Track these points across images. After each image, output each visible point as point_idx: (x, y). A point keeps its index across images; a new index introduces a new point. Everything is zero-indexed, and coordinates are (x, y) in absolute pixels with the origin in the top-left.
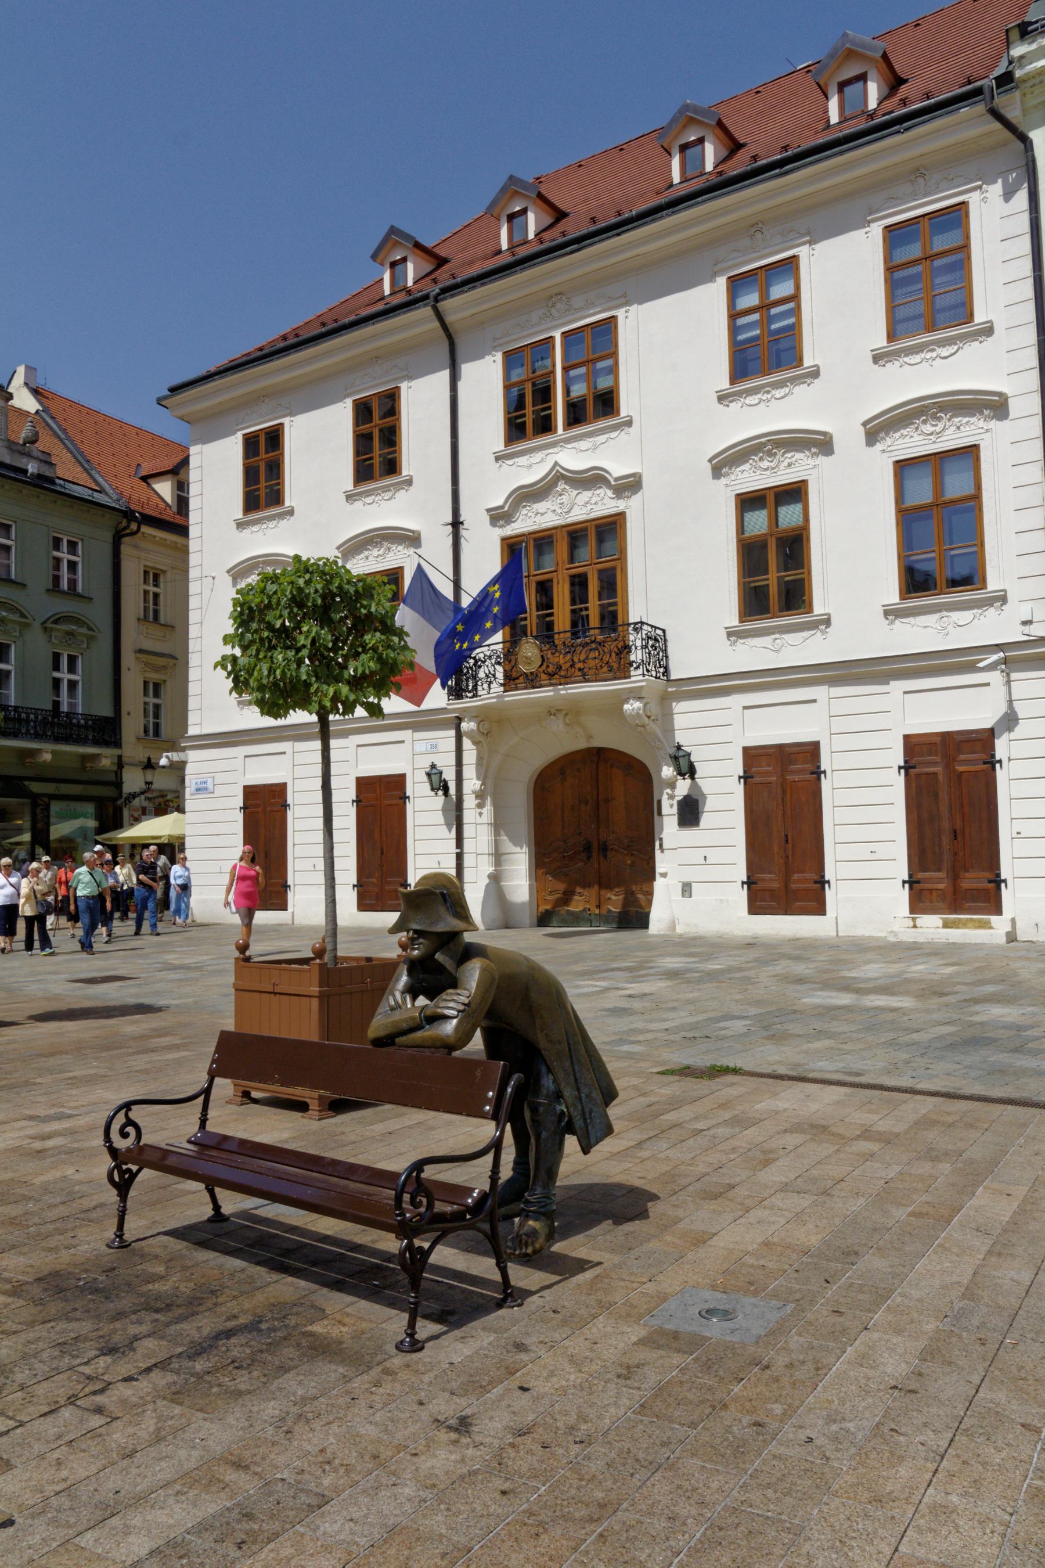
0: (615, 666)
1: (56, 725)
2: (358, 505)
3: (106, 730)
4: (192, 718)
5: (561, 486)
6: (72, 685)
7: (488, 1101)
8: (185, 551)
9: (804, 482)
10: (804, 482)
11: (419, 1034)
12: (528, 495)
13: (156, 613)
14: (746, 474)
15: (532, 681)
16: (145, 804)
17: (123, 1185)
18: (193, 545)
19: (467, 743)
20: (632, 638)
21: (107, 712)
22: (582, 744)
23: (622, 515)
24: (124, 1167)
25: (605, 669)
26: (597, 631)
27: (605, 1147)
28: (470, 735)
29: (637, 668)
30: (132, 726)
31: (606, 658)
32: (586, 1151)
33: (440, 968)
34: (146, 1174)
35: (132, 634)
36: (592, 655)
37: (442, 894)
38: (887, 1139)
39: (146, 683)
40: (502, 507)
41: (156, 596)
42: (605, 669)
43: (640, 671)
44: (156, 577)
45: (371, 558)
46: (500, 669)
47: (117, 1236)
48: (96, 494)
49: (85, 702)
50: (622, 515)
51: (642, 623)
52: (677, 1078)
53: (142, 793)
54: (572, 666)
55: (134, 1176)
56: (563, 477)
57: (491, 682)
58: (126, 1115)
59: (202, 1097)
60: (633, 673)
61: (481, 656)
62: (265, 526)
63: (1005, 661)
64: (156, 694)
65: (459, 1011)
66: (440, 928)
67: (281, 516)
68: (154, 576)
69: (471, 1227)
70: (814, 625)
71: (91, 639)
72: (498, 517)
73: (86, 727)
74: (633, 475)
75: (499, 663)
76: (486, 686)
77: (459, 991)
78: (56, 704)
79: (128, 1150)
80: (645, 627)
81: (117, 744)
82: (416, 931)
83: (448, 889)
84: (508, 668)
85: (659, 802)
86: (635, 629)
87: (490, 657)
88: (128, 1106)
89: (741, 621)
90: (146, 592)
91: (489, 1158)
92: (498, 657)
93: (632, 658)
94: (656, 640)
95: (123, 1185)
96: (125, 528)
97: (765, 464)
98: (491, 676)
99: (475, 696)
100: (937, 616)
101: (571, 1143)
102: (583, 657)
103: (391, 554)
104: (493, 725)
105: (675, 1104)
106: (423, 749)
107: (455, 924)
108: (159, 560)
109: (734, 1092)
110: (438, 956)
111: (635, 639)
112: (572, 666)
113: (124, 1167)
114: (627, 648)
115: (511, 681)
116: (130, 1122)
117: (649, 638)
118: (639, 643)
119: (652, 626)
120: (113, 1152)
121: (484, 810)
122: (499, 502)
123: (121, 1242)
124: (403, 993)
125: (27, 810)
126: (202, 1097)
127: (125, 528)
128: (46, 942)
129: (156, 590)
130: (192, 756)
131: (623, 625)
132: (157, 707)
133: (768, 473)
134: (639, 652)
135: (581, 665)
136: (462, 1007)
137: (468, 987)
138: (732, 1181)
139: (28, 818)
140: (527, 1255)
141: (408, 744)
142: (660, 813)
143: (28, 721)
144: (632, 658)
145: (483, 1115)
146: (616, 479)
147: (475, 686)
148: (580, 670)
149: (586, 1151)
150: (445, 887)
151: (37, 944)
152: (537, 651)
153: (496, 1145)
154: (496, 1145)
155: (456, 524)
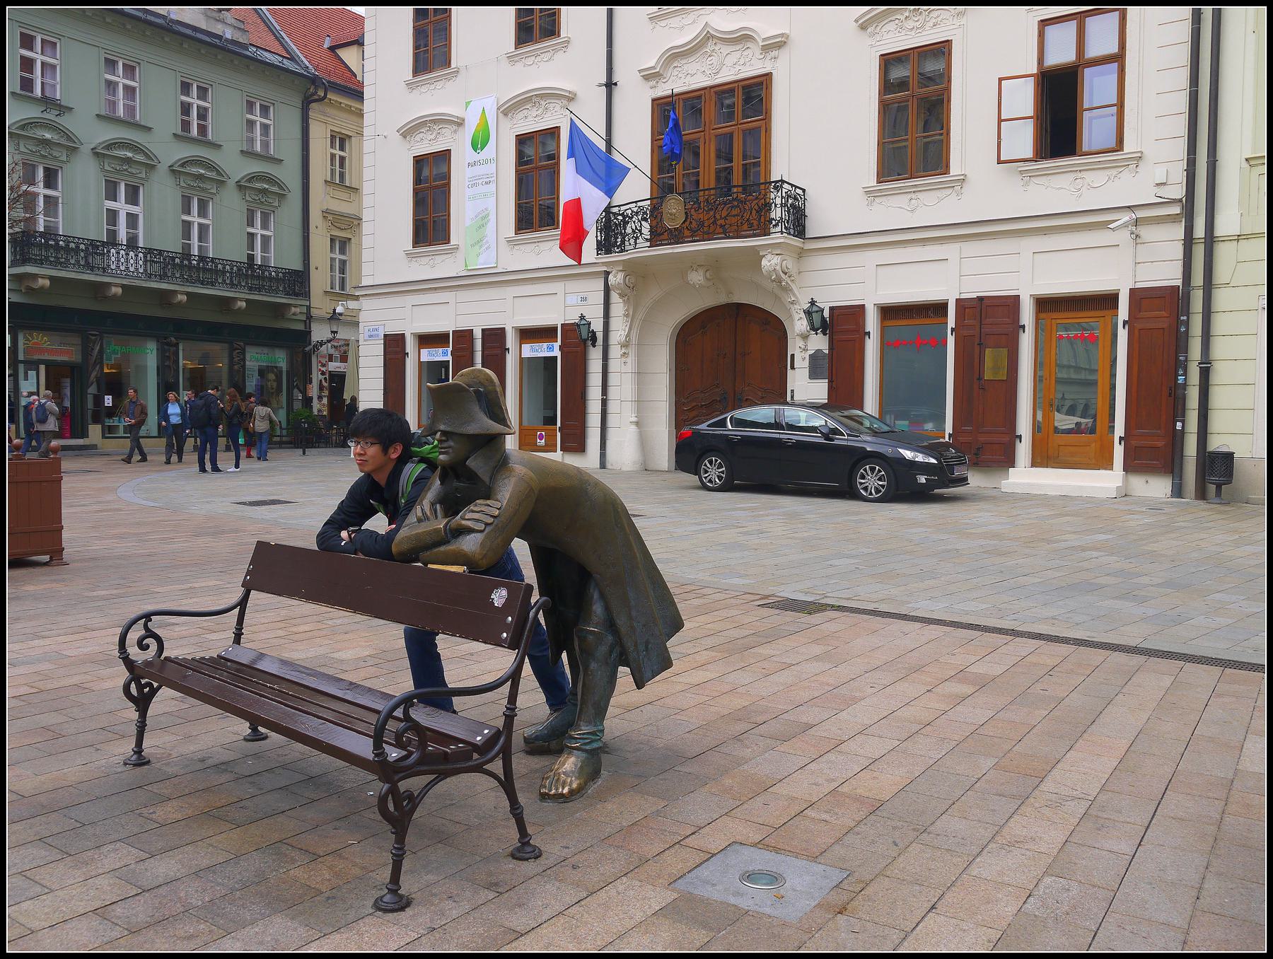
0: (755, 223)
1: (250, 273)
2: (519, 66)
3: (298, 281)
4: (366, 270)
5: (710, 47)
6: (266, 240)
7: (506, 628)
8: (360, 114)
9: (948, 42)
10: (948, 43)
11: (442, 548)
12: (675, 56)
13: (342, 175)
14: (891, 35)
15: (676, 237)
16: (332, 351)
17: (142, 702)
18: (368, 106)
19: (615, 297)
20: (772, 196)
21: (296, 265)
22: (722, 299)
23: (768, 76)
24: (143, 682)
25: (745, 227)
26: (740, 189)
27: (656, 686)
28: (618, 287)
29: (776, 225)
30: (320, 280)
31: (746, 215)
32: (640, 685)
33: (472, 477)
34: (165, 692)
35: (320, 198)
36: (735, 212)
37: (477, 392)
38: (983, 683)
39: (332, 240)
40: (653, 68)
41: (342, 159)
42: (745, 227)
43: (779, 229)
44: (342, 141)
45: (530, 118)
46: (646, 225)
47: (135, 753)
48: (285, 61)
49: (283, 257)
50: (768, 76)
51: (783, 181)
52: (777, 611)
53: (329, 341)
54: (715, 223)
55: (154, 692)
56: (713, 36)
57: (637, 238)
58: (146, 626)
59: (236, 611)
60: (773, 230)
61: (629, 212)
62: (432, 87)
63: (1137, 222)
64: (342, 251)
65: (487, 524)
66: (472, 429)
67: (448, 78)
68: (341, 140)
69: (478, 769)
70: (951, 185)
71: (282, 197)
72: (651, 76)
73: (277, 280)
74: (782, 35)
75: (645, 220)
76: (632, 241)
77: (488, 502)
78: (251, 258)
79: (147, 664)
80: (785, 186)
81: (307, 295)
82: (444, 433)
83: (485, 387)
84: (654, 224)
85: (793, 356)
86: (775, 188)
87: (637, 213)
88: (148, 616)
89: (879, 182)
90: (333, 156)
91: (506, 688)
92: (645, 213)
93: (773, 215)
94: (795, 199)
95: (142, 702)
96: (313, 94)
97: (910, 24)
98: (637, 232)
99: (622, 251)
100: (1071, 176)
101: (623, 671)
102: (724, 213)
103: (549, 114)
104: (639, 275)
105: (770, 637)
106: (574, 302)
107: (496, 427)
108: (343, 124)
109: (831, 627)
110: (471, 463)
111: (777, 198)
112: (715, 223)
113: (143, 682)
114: (767, 206)
115: (657, 237)
116: (151, 634)
117: (789, 196)
118: (778, 201)
119: (792, 185)
120: (129, 663)
121: (629, 360)
122: (652, 64)
123: (140, 759)
124: (433, 504)
125: (226, 354)
126: (236, 611)
127: (313, 94)
128: (216, 469)
129: (342, 154)
130: (365, 304)
131: (765, 183)
132: (343, 263)
133: (913, 33)
134: (779, 210)
135: (722, 222)
136: (490, 520)
137: (499, 497)
138: (811, 721)
139: (226, 361)
140: (562, 795)
141: (561, 296)
142: (793, 368)
143: (224, 272)
144: (773, 215)
145: (498, 643)
146: (764, 40)
147: (623, 242)
148: (721, 226)
149: (640, 685)
150: (481, 384)
151: (208, 466)
152: (681, 207)
153: (515, 676)
154: (515, 676)
155: (610, 85)
